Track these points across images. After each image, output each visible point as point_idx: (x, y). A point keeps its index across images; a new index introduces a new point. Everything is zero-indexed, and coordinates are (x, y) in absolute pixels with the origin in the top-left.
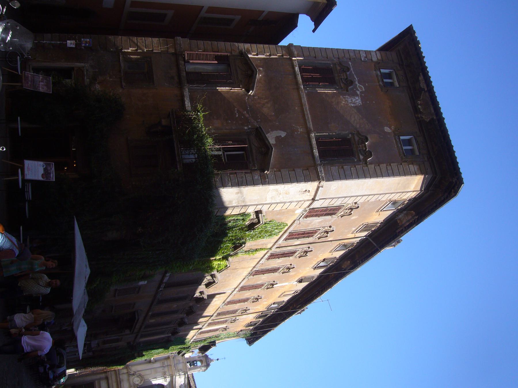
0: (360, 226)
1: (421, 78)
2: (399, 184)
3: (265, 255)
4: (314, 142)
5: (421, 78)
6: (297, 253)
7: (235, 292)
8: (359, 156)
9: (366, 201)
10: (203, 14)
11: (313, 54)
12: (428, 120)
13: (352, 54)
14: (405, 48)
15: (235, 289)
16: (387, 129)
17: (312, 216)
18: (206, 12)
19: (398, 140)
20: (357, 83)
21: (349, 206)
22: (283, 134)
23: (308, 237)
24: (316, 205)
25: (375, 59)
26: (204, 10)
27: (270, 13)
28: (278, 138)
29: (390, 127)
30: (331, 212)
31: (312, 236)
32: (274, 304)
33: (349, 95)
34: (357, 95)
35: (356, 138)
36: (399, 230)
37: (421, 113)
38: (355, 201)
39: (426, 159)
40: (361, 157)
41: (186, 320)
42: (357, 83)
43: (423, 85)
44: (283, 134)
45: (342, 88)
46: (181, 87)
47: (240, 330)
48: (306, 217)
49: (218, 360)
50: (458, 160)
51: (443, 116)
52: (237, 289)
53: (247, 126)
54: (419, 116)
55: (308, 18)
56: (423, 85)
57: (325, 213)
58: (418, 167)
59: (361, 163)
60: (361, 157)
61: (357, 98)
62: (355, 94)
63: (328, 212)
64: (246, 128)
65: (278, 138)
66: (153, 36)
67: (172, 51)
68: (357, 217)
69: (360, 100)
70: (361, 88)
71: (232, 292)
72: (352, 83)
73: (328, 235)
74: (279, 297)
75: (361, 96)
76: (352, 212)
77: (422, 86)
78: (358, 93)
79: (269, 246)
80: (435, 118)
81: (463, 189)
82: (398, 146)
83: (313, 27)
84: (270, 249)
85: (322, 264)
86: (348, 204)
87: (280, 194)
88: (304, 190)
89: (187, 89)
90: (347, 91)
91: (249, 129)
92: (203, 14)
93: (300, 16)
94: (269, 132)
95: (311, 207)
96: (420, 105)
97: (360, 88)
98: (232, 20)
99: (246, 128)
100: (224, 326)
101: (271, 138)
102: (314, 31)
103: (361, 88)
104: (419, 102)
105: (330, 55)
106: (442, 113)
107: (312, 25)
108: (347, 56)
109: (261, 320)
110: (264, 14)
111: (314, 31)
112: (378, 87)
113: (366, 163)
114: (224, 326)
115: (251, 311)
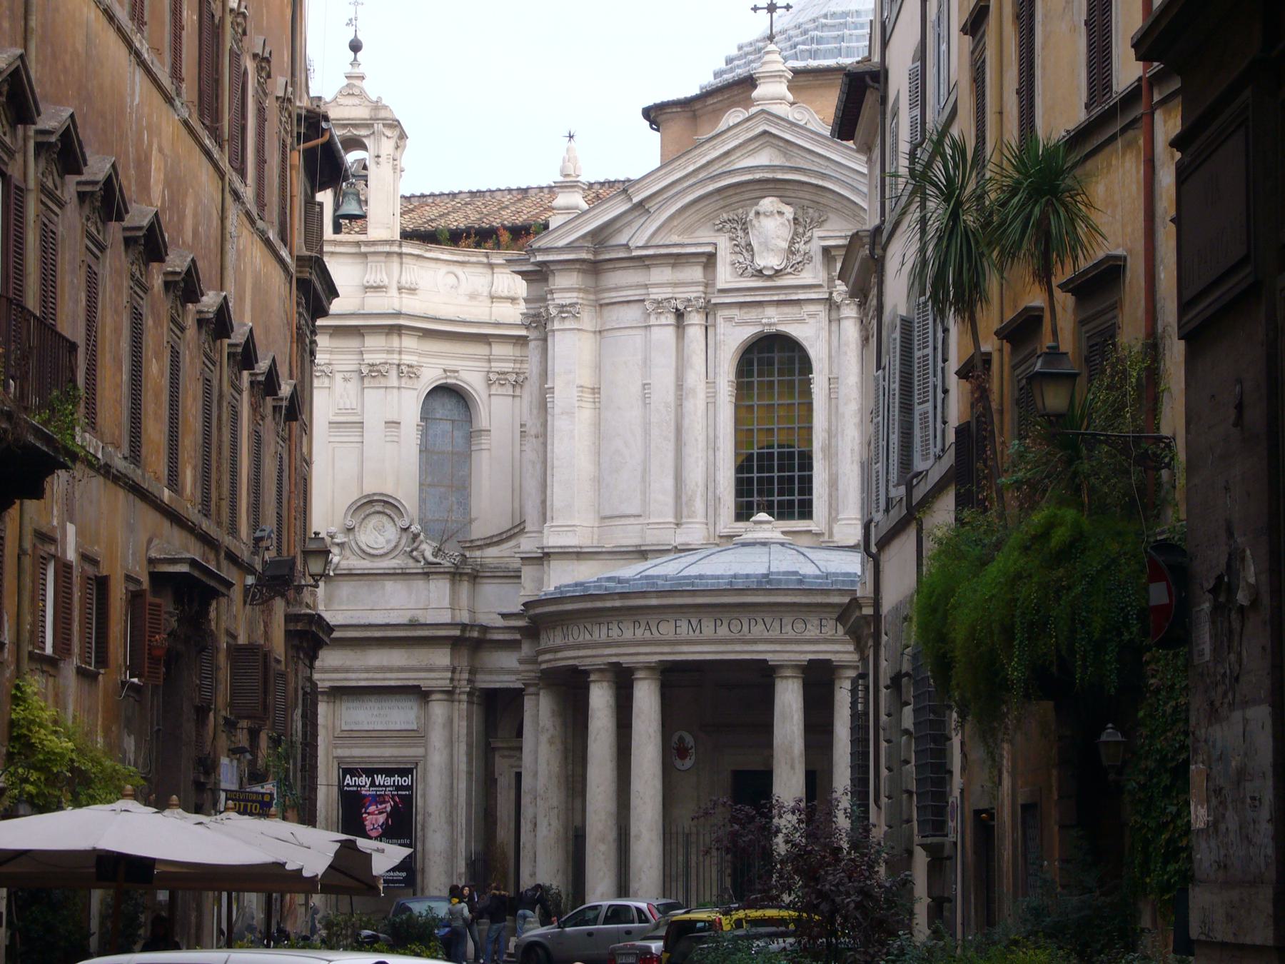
49: (355, 47)
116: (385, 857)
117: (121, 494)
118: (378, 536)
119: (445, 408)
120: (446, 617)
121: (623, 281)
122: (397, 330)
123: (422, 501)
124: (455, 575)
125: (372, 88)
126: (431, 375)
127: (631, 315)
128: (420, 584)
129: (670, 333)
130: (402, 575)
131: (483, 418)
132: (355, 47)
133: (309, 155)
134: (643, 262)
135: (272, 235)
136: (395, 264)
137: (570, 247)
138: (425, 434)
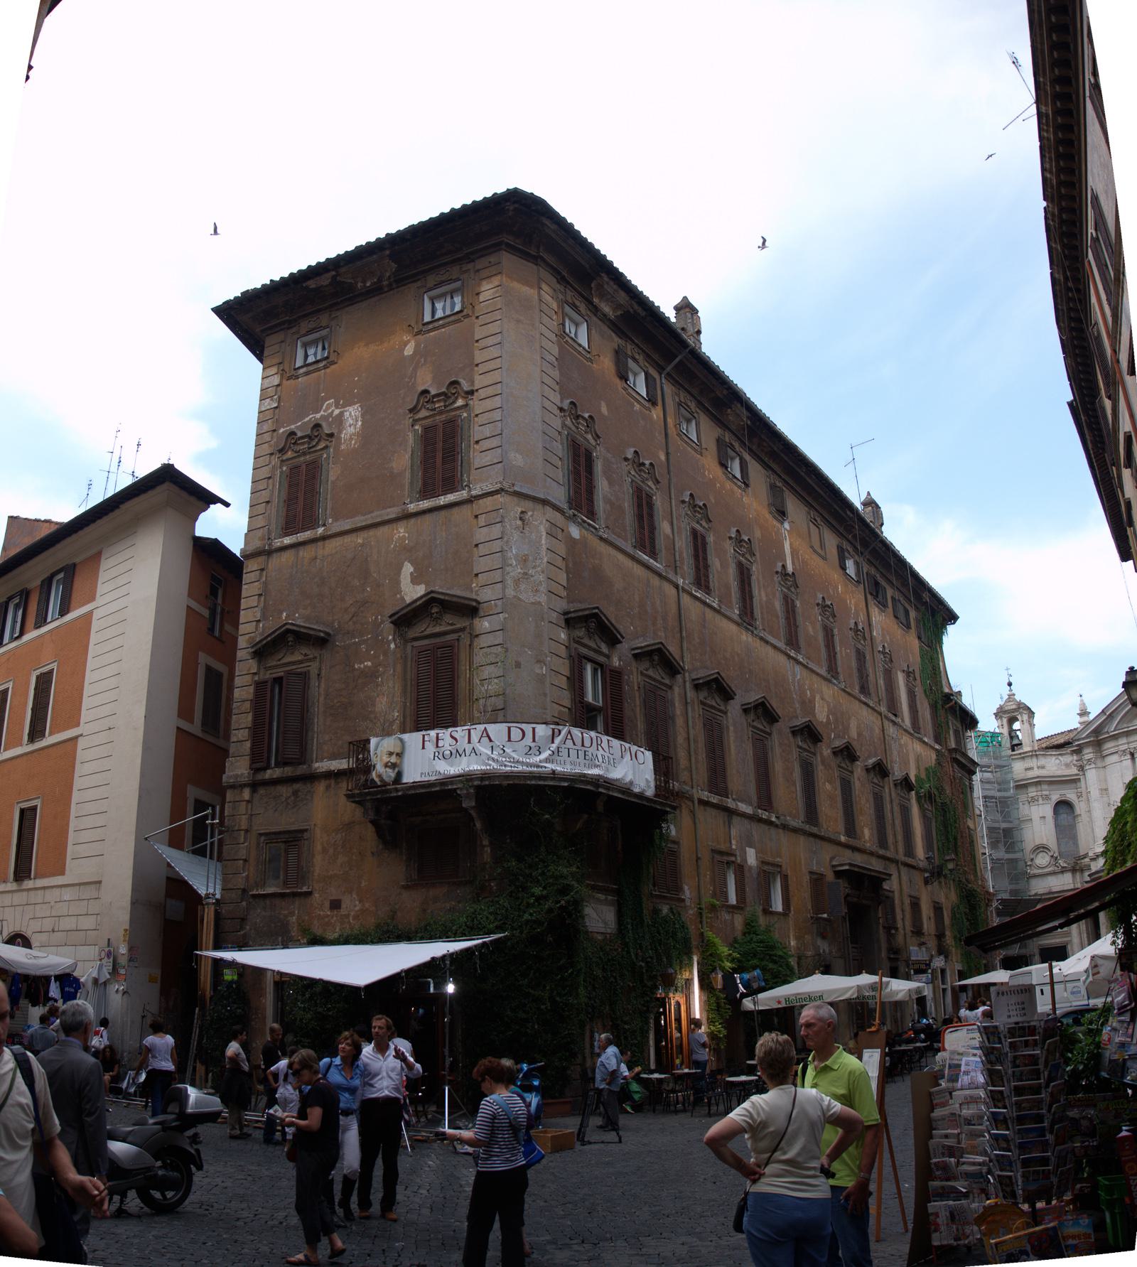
0: (629, 394)
1: (312, 284)
2: (518, 321)
3: (696, 598)
4: (425, 504)
5: (312, 284)
6: (697, 527)
7: (800, 658)
8: (459, 408)
9: (557, 388)
10: (195, 728)
11: (261, 508)
12: (394, 266)
13: (266, 427)
14: (261, 317)
15: (789, 657)
16: (409, 350)
17: (591, 501)
18: (192, 722)
19: (431, 326)
20: (318, 416)
21: (568, 422)
22: (408, 569)
23: (651, 506)
24: (559, 495)
25: (276, 380)
26: (185, 725)
27: (190, 595)
28: (415, 580)
29: (406, 344)
30: (583, 460)
31: (649, 497)
32: (844, 568)
33: (340, 432)
34: (341, 414)
35: (423, 413)
36: (640, 311)
37: (380, 280)
38: (557, 412)
39: (470, 266)
40: (460, 402)
41: (871, 761)
42: (318, 416)
43: (325, 280)
44: (408, 569)
45: (326, 447)
46: (312, 778)
47: (917, 641)
48: (592, 514)
49: (1010, 684)
50: (469, 202)
51: (382, 236)
52: (792, 654)
53: (389, 643)
54: (385, 283)
55: (203, 516)
56: (325, 280)
57: (583, 474)
58: (484, 283)
59: (471, 402)
60: (460, 402)
61: (347, 414)
62: (340, 420)
63: (582, 469)
64: (392, 646)
65: (415, 580)
66: (657, 770)
67: (246, 794)
68: (603, 404)
69: (351, 409)
70: (328, 408)
71: (799, 662)
72: (317, 426)
73: (647, 462)
74: (824, 558)
75: (343, 407)
76: (586, 415)
77: (327, 282)
78: (337, 412)
79: (674, 591)
80: (388, 252)
81: (527, 188)
82: (443, 326)
83: (219, 505)
84: (677, 587)
85: (736, 468)
86: (564, 425)
87: (525, 574)
88: (519, 522)
89: (317, 765)
90: (331, 435)
91: (394, 639)
92: (195, 728)
93: (197, 534)
94: (403, 599)
95: (565, 506)
96: (364, 282)
97: (329, 409)
98: (209, 669)
99: (392, 646)
100: (901, 679)
101: (412, 592)
102: (227, 505)
103: (328, 408)
104: (359, 285)
105: (265, 472)
106: (378, 239)
107: (215, 509)
108: (267, 437)
109: (890, 592)
110: (194, 605)
111: (227, 505)
112: (328, 370)
113: (471, 393)
114: (901, 679)
115: (862, 617)
116: (420, 1108)
117: (802, 838)
118: (1042, 860)
119: (1062, 809)
120: (1072, 887)
121: (1109, 746)
122: (1039, 783)
123: (1059, 845)
124: (1074, 870)
125: (1018, 698)
126: (1055, 797)
127: (1115, 758)
128: (1060, 876)
129: (1129, 762)
130: (1054, 873)
131: (1078, 811)
132: (1010, 684)
133: (428, 438)
134: (1115, 737)
135: (883, 709)
136: (1034, 759)
137: (1087, 737)
138: (1056, 820)
